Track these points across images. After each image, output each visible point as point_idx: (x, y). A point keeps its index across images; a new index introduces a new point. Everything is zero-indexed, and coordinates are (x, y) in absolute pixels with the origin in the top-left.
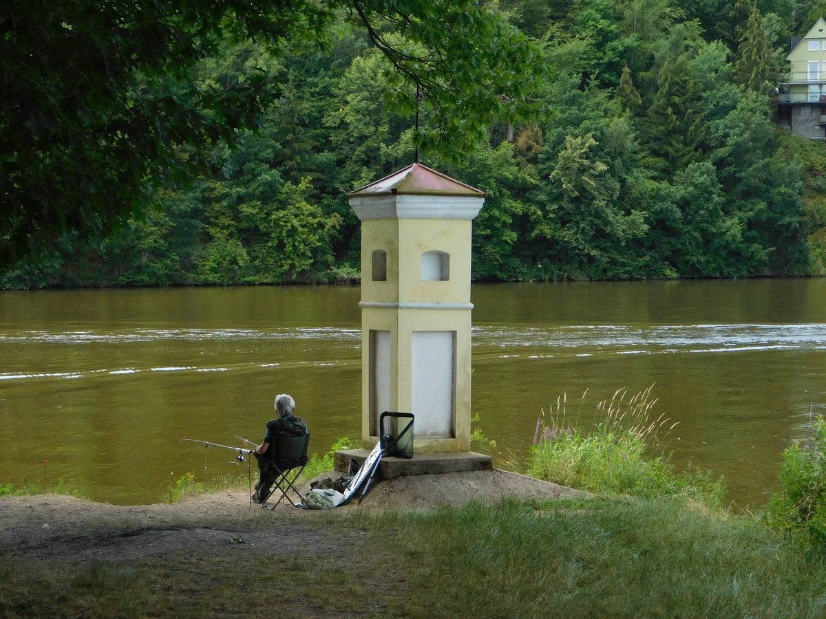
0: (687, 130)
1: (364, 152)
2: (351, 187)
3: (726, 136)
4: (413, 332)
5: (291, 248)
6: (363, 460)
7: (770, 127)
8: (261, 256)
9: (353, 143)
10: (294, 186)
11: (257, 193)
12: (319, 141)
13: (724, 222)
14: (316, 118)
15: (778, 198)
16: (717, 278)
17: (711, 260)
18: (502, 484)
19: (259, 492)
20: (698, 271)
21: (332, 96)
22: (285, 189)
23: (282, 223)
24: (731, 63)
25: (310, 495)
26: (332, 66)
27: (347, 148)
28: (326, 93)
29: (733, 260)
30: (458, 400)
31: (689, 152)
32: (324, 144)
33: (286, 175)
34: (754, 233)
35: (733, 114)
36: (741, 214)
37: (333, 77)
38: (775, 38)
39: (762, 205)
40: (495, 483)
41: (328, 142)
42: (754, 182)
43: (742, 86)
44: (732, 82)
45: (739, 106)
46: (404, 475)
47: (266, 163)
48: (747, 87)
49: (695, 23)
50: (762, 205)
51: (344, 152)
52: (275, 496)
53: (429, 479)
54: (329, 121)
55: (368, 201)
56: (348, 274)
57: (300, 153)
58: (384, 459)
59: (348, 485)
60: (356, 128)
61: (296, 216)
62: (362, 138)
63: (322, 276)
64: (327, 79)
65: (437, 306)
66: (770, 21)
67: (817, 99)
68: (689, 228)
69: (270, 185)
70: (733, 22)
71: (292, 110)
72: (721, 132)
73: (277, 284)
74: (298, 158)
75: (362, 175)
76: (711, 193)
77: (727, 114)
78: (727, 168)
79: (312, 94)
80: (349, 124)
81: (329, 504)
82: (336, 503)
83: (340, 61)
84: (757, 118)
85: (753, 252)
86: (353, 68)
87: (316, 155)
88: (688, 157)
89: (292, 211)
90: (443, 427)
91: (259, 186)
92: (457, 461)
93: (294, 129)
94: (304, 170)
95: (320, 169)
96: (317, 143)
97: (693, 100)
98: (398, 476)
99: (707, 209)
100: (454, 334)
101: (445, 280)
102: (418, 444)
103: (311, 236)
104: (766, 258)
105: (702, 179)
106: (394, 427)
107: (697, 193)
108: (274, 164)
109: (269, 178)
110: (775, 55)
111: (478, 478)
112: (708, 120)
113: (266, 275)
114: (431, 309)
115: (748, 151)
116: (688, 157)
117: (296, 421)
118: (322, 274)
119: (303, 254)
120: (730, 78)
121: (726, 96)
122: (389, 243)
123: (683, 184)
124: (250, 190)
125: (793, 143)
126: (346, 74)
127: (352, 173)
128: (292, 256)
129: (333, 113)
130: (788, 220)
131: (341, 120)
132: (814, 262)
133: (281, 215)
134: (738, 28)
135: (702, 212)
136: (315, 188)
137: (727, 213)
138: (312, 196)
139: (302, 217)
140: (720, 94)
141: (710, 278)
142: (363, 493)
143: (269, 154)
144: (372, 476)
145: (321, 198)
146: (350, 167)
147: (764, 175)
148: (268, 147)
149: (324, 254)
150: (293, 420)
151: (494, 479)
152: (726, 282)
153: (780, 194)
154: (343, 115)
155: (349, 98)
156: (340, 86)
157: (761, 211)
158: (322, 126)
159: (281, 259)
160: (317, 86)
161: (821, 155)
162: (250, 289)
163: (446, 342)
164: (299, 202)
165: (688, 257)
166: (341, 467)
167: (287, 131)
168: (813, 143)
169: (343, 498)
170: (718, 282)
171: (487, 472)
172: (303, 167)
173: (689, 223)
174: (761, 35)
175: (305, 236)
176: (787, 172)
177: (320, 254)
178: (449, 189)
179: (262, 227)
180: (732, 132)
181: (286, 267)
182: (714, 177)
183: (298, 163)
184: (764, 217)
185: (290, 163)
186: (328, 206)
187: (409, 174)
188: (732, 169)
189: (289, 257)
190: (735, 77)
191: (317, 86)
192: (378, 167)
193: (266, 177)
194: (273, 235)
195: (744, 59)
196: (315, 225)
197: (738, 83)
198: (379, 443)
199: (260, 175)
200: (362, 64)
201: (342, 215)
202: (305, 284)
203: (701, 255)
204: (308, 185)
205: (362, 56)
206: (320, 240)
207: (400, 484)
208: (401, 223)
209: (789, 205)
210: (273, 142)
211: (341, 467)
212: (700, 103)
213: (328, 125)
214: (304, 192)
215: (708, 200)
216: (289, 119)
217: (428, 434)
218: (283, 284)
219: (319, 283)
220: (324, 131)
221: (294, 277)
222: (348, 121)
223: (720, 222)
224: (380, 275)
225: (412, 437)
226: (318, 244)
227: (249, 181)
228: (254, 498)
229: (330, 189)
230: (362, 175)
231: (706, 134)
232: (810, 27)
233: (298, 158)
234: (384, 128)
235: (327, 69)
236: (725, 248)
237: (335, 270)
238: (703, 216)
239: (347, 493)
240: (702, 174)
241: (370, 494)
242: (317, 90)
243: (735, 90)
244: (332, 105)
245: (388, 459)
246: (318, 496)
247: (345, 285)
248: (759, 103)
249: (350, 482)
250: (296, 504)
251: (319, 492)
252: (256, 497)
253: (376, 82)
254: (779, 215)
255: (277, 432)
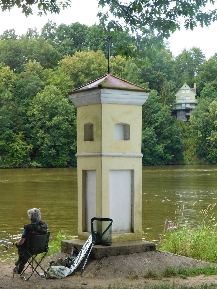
0: (145, 117)
1: (41, 124)
2: (36, 136)
3: (157, 119)
4: (110, 170)
5: (16, 156)
6: (81, 247)
7: (171, 116)
8: (6, 159)
9: (37, 121)
10: (17, 135)
11: (4, 138)
12: (25, 121)
13: (157, 147)
14: (24, 113)
15: (174, 139)
16: (155, 165)
17: (153, 159)
18: (163, 260)
19: (18, 267)
20: (149, 163)
21: (30, 106)
22: (14, 136)
23: (13, 148)
24: (158, 96)
25: (50, 270)
26: (30, 96)
27: (34, 123)
28: (28, 105)
29: (160, 159)
30: (135, 210)
31: (146, 125)
32: (27, 121)
33: (14, 132)
34: (167, 151)
35: (159, 112)
36: (163, 144)
37: (30, 99)
38: (172, 88)
39: (169, 142)
40: (159, 259)
41: (28, 121)
42: (167, 134)
43: (162, 103)
44: (159, 102)
45: (161, 110)
46: (106, 256)
47: (8, 128)
48: (164, 104)
49: (147, 83)
50: (169, 142)
51: (34, 124)
52: (28, 270)
53: (121, 258)
54: (29, 114)
55: (81, 95)
56: (35, 164)
57: (19, 124)
58: (95, 247)
59: (73, 263)
60: (38, 116)
61: (18, 145)
62: (40, 120)
63: (26, 165)
64: (28, 100)
65: (123, 155)
66: (170, 83)
67: (184, 108)
68: (146, 149)
69: (9, 135)
70: (159, 83)
71: (16, 110)
72: (156, 118)
73: (11, 168)
74: (18, 126)
75: (40, 132)
76: (153, 138)
77: (157, 112)
78: (158, 130)
79: (23, 105)
80: (35, 115)
81: (63, 276)
82: (66, 275)
83: (32, 94)
84: (167, 114)
85: (166, 157)
86: (37, 96)
87: (24, 125)
88: (145, 126)
89: (16, 144)
90: (127, 226)
91: (5, 135)
92: (136, 247)
93: (17, 117)
94: (20, 130)
95: (26, 130)
96: (25, 121)
97: (146, 108)
98: (103, 257)
99: (152, 143)
100: (132, 172)
101: (127, 140)
102: (114, 237)
103: (23, 152)
104: (171, 159)
105: (150, 133)
106: (99, 227)
107: (149, 137)
108: (10, 128)
109: (9, 133)
110: (172, 94)
111: (149, 256)
112: (152, 114)
113: (8, 165)
114: (120, 156)
115: (164, 124)
116: (145, 126)
117: (42, 225)
118: (26, 164)
119: (20, 158)
120: (158, 101)
121: (157, 107)
122: (95, 118)
123: (144, 135)
124: (2, 137)
125: (177, 122)
126: (34, 98)
127: (37, 131)
128: (16, 159)
129: (30, 111)
130: (178, 146)
131: (33, 114)
132: (186, 160)
133: (13, 145)
134: (160, 85)
135: (150, 144)
136: (24, 136)
137: (158, 144)
138: (23, 139)
139: (20, 145)
140: (155, 106)
141: (153, 165)
142: (83, 268)
143: (9, 124)
144: (88, 257)
145: (26, 139)
146: (36, 129)
147: (170, 132)
148: (8, 122)
149: (27, 158)
150: (41, 223)
151: (158, 256)
152: (158, 166)
153: (175, 138)
154: (33, 112)
155: (35, 106)
156: (32, 103)
157: (169, 143)
158: (27, 116)
159: (12, 160)
160: (25, 103)
161: (186, 126)
162: (2, 169)
163: (128, 175)
164: (19, 140)
165: (146, 158)
166: (66, 250)
167: (15, 117)
168: (184, 122)
169: (71, 271)
170: (155, 166)
171: (153, 252)
172: (20, 129)
173: (146, 147)
174: (168, 87)
175: (21, 152)
176: (177, 131)
177: (26, 158)
178: (130, 87)
179: (6, 149)
180: (159, 118)
181: (14, 162)
182: (154, 133)
183: (18, 128)
184: (170, 145)
185: (15, 128)
186: (28, 142)
187: (106, 78)
188: (160, 130)
189: (15, 159)
190: (160, 101)
191: (25, 103)
192: (45, 129)
193: (8, 132)
194: (10, 152)
195: (163, 95)
196: (24, 148)
197: (161, 103)
198: (91, 236)
199: (5, 131)
200: (40, 95)
201: (33, 145)
202: (21, 168)
203: (150, 158)
204: (22, 135)
205: (39, 93)
206: (26, 153)
207: (105, 262)
208: (103, 105)
209: (178, 142)
210: (10, 121)
211: (66, 250)
212: (149, 109)
213: (28, 115)
214: (20, 137)
215: (152, 140)
216: (15, 113)
217: (119, 230)
218: (13, 168)
219: (25, 167)
220: (27, 117)
221: (17, 165)
222: (35, 114)
223: (156, 147)
224: (89, 137)
225: (111, 232)
226: (26, 154)
227: (2, 134)
228: (14, 270)
229: (29, 136)
230: (40, 132)
231: (151, 119)
232: (182, 86)
233: (18, 126)
234: (47, 116)
235: (28, 97)
236: (158, 155)
237: (31, 163)
238: (151, 145)
239: (73, 268)
240: (150, 131)
241: (87, 269)
242: (25, 104)
243: (160, 105)
244: (30, 109)
245: (98, 247)
246: (55, 270)
247: (34, 168)
248: (168, 109)
249: (74, 260)
250: (41, 274)
251: (56, 268)
252: (16, 269)
253: (45, 101)
254: (174, 145)
255: (30, 232)
